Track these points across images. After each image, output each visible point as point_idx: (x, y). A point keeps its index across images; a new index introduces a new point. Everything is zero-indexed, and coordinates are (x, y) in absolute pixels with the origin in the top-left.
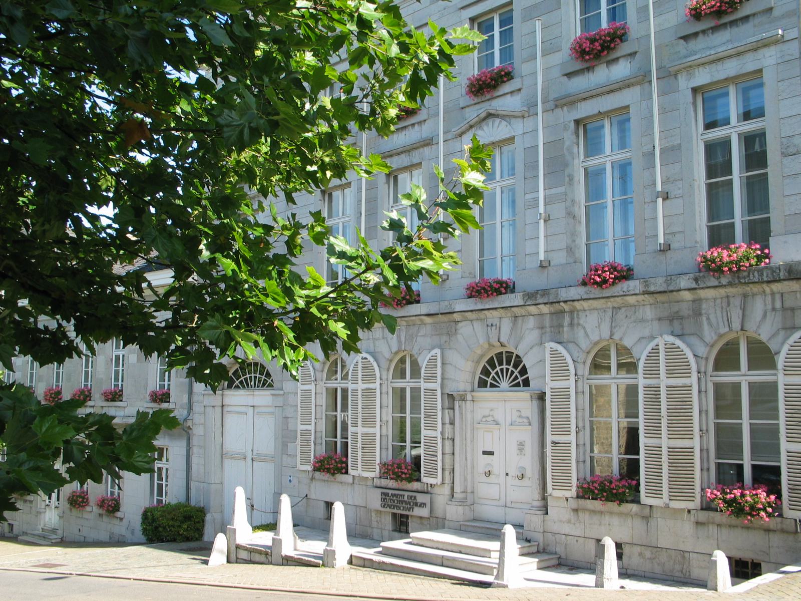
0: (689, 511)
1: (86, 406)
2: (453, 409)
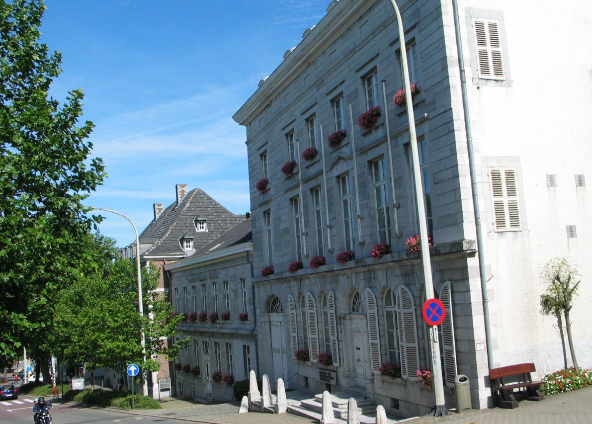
0: (416, 382)
1: (216, 323)
2: (341, 324)
